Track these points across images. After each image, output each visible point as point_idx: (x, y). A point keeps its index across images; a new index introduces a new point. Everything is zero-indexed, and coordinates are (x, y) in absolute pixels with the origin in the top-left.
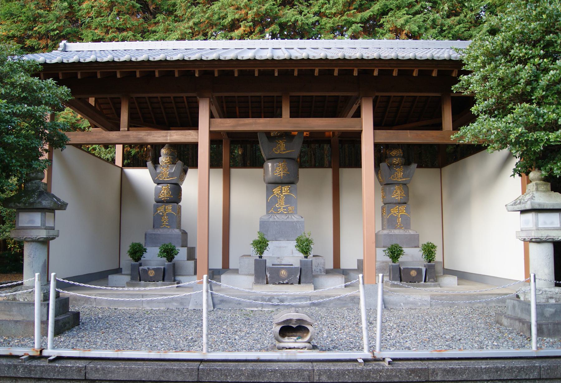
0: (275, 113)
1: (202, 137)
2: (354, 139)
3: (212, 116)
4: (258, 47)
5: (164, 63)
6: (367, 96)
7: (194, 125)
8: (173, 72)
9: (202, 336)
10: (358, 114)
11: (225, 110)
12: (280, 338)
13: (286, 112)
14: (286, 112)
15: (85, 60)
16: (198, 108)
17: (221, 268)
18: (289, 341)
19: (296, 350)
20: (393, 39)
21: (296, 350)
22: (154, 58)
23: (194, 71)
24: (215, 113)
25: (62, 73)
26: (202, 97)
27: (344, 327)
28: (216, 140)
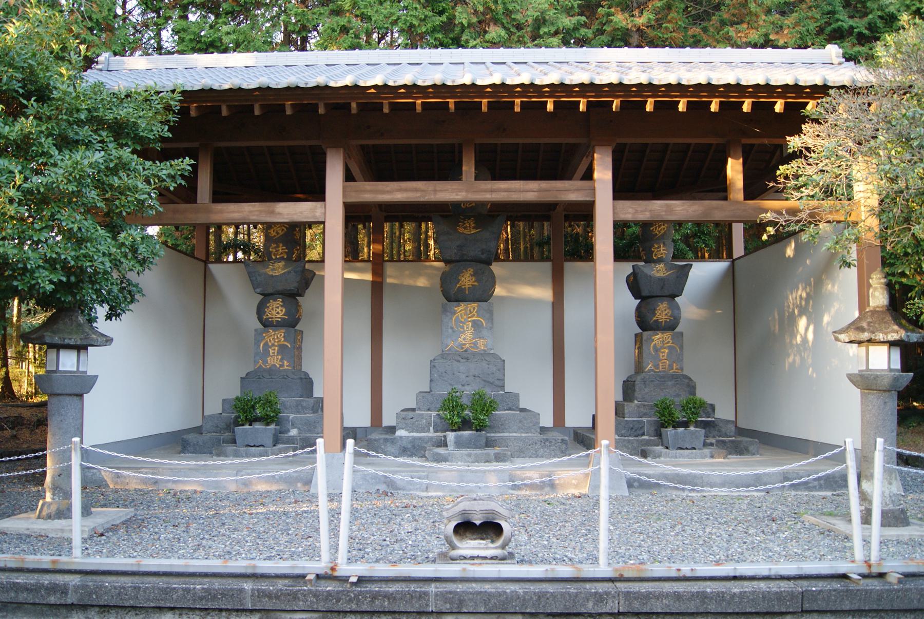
0: (451, 172)
1: (329, 213)
2: (584, 213)
3: (349, 177)
4: (446, 60)
5: (237, 93)
6: (603, 144)
7: (317, 193)
8: (316, 107)
9: (317, 530)
10: (588, 175)
11: (377, 165)
12: (455, 540)
13: (469, 168)
14: (469, 168)
15: (454, 81)
16: (325, 162)
17: (369, 425)
18: (471, 546)
19: (477, 560)
20: (559, 47)
21: (477, 560)
22: (454, 81)
23: (317, 105)
24: (356, 171)
25: (228, 106)
26: (336, 146)
27: (416, 520)
28: (355, 215)
